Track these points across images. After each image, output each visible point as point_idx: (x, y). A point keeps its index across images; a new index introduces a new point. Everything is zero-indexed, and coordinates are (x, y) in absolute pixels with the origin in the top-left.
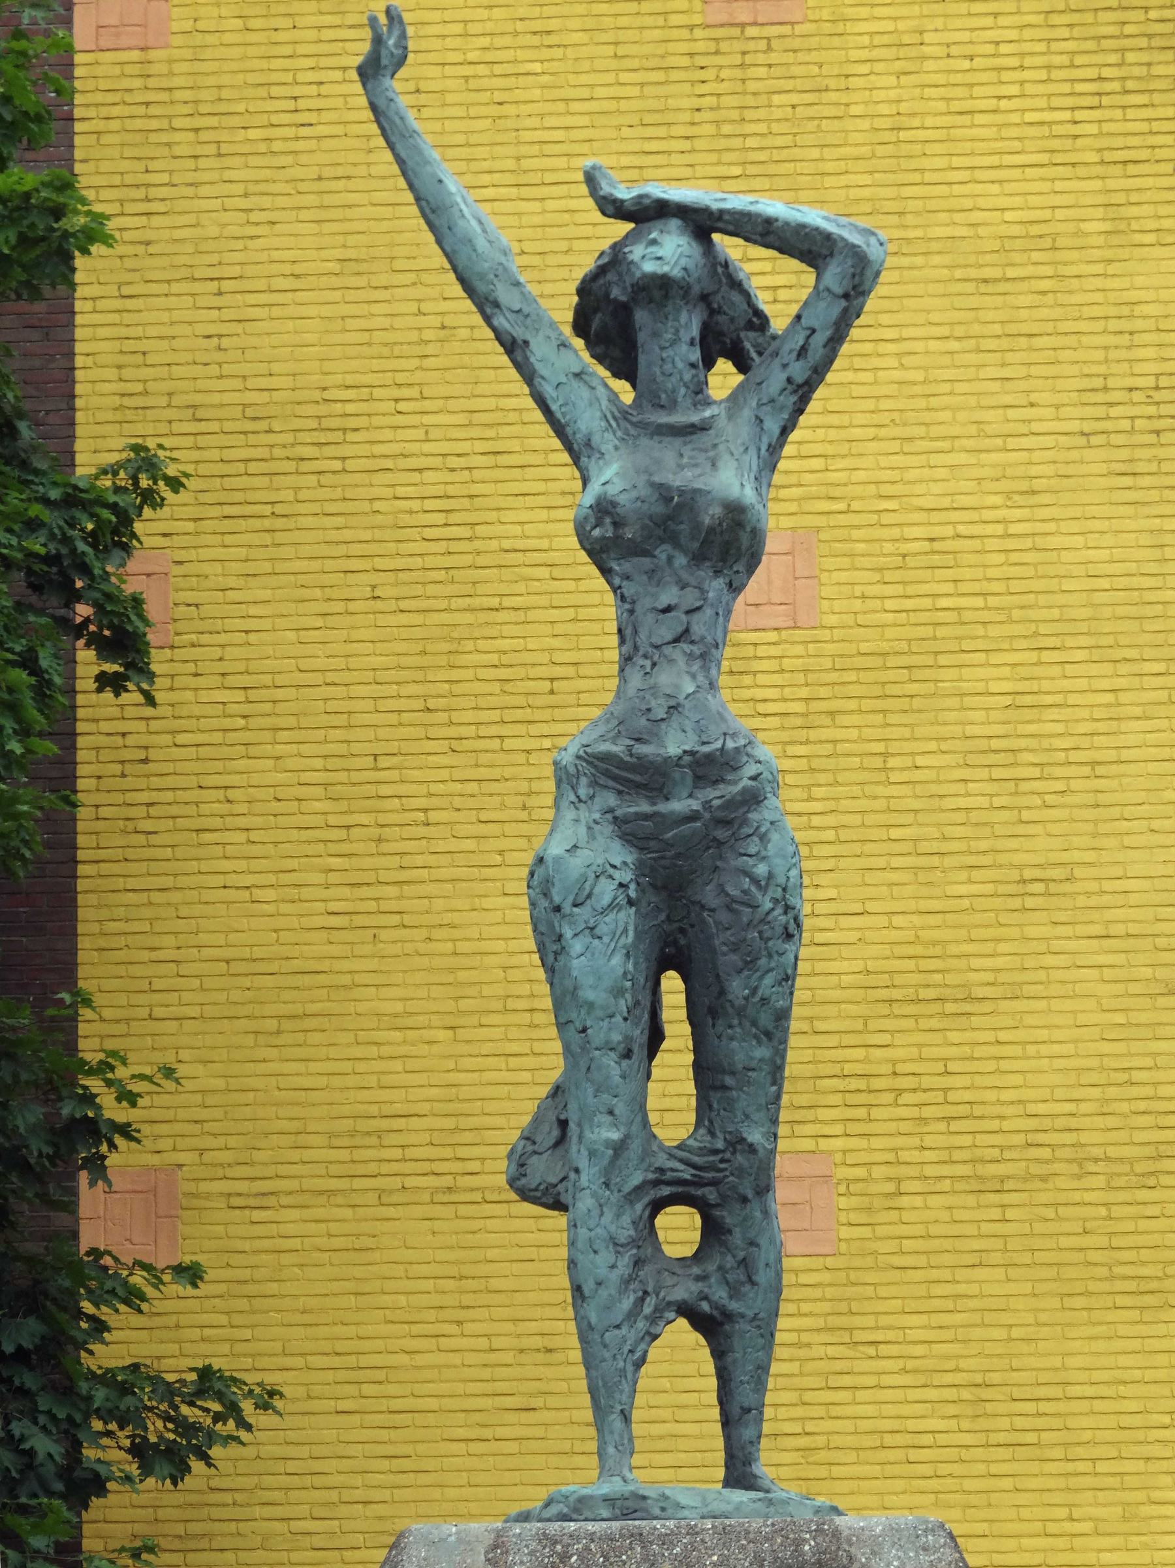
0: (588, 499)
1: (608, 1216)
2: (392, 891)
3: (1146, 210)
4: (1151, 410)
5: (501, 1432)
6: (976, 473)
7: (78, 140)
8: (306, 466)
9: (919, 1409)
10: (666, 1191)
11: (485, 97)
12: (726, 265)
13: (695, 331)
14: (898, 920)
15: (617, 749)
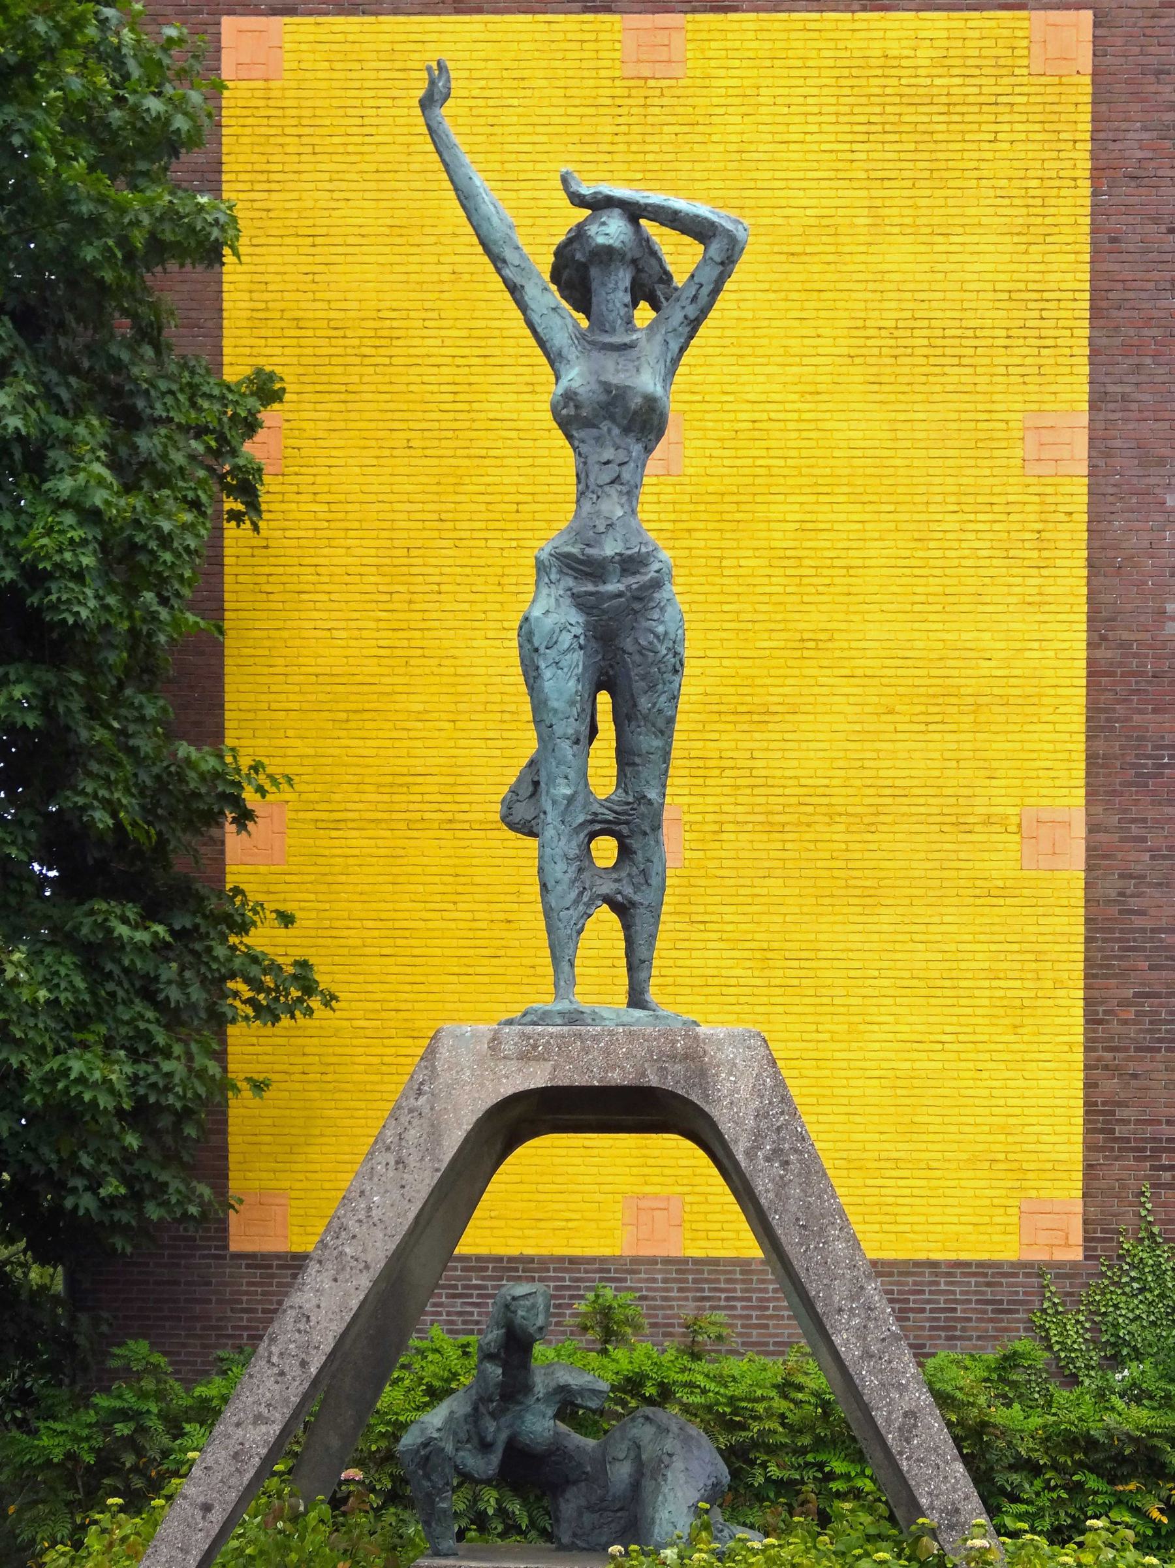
0: (560, 391)
1: (564, 840)
2: (418, 634)
3: (895, 211)
4: (892, 342)
5: (479, 970)
6: (783, 379)
7: (224, 140)
8: (367, 361)
9: (730, 963)
10: (598, 827)
11: (482, 121)
12: (648, 240)
13: (627, 283)
14: (726, 662)
15: (575, 550)
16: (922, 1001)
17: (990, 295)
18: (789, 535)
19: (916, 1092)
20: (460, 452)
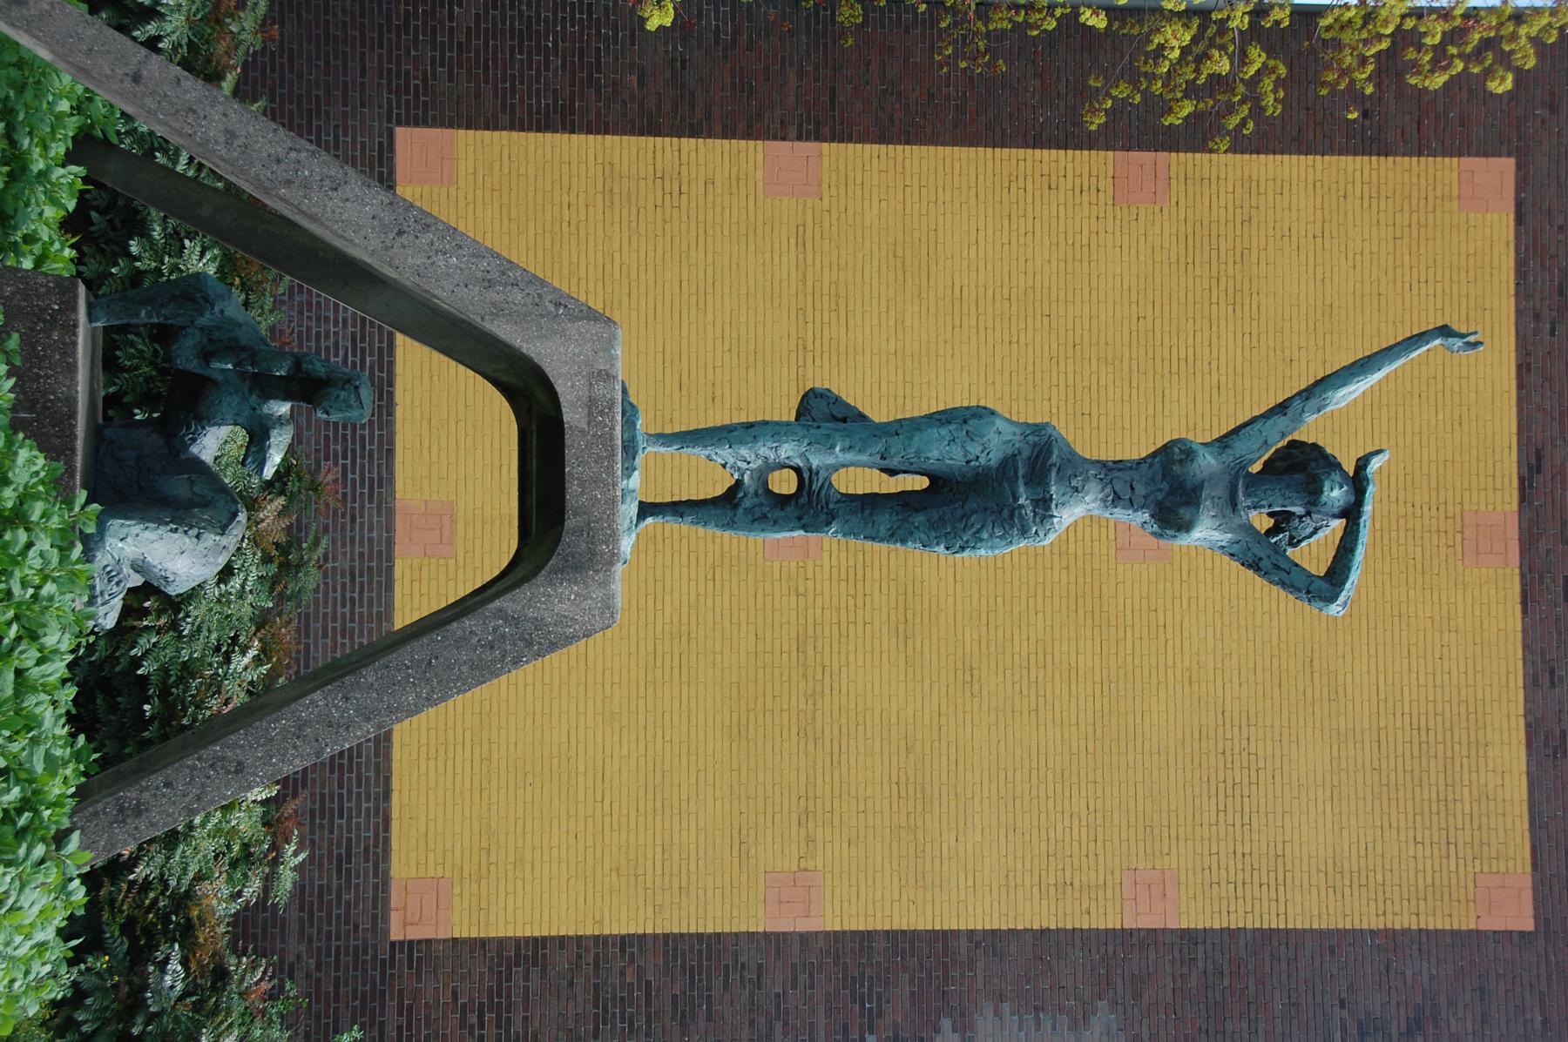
4: (1237, 751)
5: (668, 370)
7: (1407, 159)
8: (1214, 281)
10: (806, 476)
11: (1424, 388)
14: (951, 600)
16: (642, 783)
17: (1280, 839)
18: (1065, 657)
19: (556, 776)
20: (1134, 363)
